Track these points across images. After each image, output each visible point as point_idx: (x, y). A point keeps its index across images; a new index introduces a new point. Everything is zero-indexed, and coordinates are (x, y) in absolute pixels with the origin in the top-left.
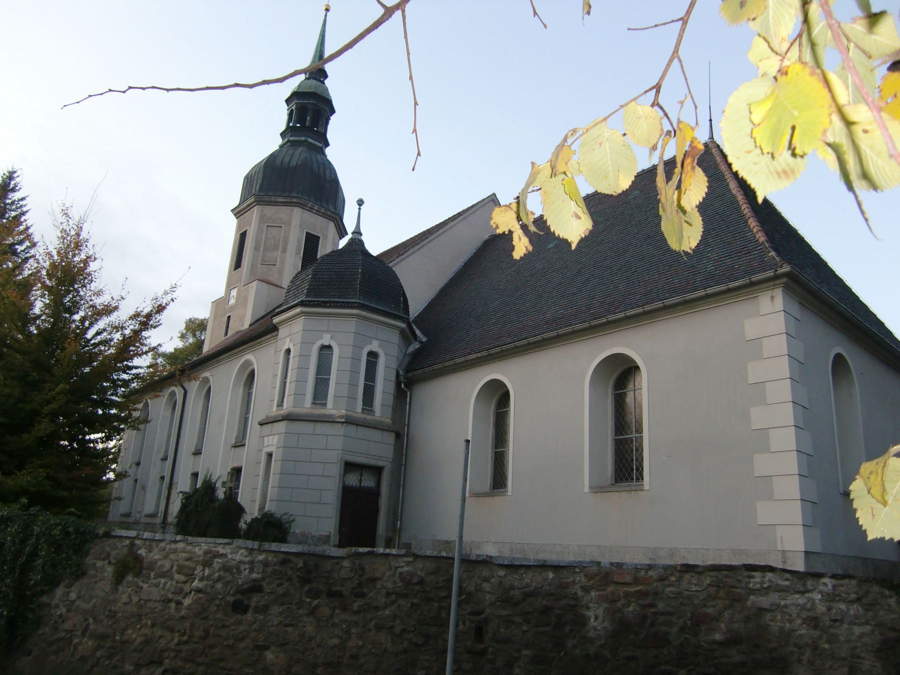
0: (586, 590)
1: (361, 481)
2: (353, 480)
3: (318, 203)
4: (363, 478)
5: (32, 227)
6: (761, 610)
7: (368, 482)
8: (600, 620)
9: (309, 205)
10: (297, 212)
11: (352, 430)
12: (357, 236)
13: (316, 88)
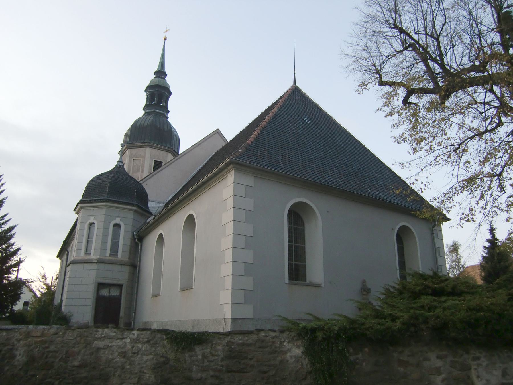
0: (19, 340)
1: (109, 293)
2: (105, 292)
3: (160, 144)
4: (110, 291)
5: (3, 175)
6: (99, 349)
7: (115, 293)
8: (21, 356)
9: (155, 146)
10: (148, 150)
11: (102, 266)
12: (121, 164)
13: (159, 82)
